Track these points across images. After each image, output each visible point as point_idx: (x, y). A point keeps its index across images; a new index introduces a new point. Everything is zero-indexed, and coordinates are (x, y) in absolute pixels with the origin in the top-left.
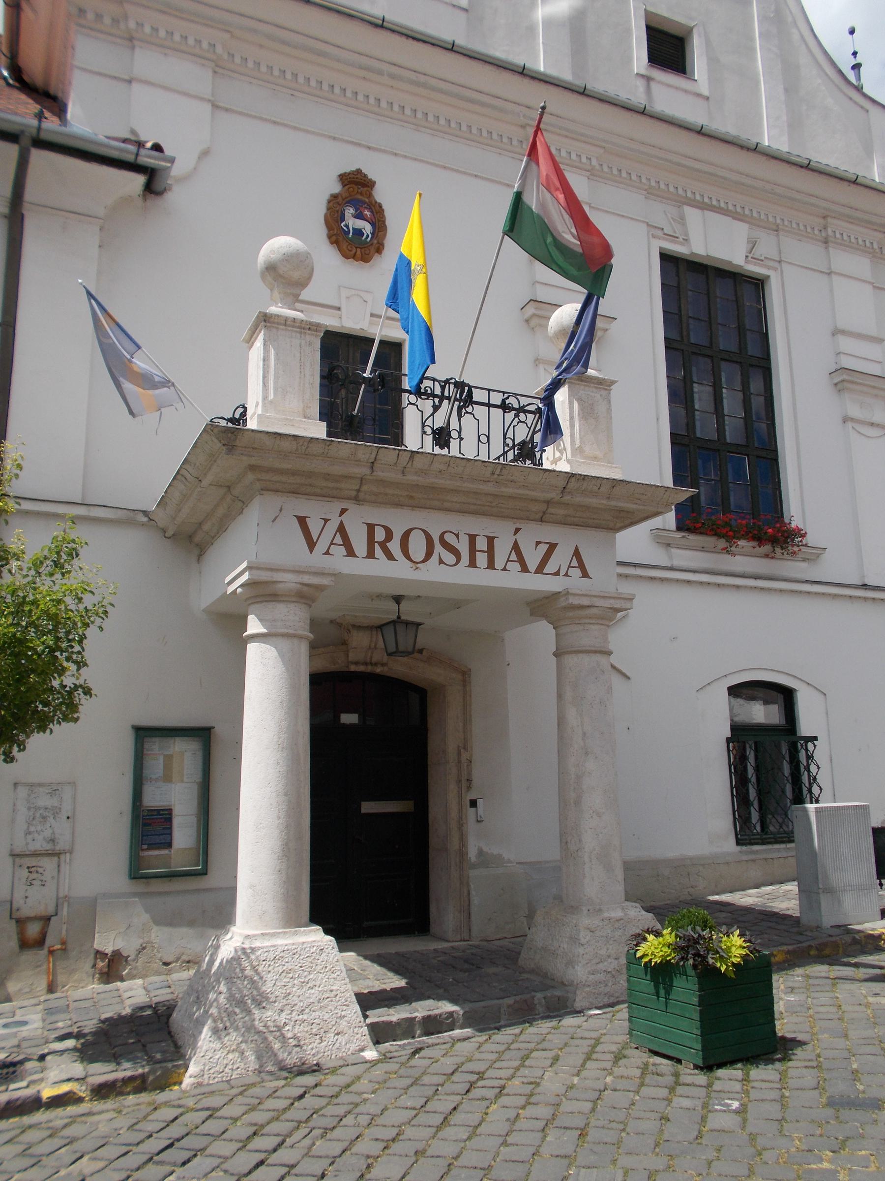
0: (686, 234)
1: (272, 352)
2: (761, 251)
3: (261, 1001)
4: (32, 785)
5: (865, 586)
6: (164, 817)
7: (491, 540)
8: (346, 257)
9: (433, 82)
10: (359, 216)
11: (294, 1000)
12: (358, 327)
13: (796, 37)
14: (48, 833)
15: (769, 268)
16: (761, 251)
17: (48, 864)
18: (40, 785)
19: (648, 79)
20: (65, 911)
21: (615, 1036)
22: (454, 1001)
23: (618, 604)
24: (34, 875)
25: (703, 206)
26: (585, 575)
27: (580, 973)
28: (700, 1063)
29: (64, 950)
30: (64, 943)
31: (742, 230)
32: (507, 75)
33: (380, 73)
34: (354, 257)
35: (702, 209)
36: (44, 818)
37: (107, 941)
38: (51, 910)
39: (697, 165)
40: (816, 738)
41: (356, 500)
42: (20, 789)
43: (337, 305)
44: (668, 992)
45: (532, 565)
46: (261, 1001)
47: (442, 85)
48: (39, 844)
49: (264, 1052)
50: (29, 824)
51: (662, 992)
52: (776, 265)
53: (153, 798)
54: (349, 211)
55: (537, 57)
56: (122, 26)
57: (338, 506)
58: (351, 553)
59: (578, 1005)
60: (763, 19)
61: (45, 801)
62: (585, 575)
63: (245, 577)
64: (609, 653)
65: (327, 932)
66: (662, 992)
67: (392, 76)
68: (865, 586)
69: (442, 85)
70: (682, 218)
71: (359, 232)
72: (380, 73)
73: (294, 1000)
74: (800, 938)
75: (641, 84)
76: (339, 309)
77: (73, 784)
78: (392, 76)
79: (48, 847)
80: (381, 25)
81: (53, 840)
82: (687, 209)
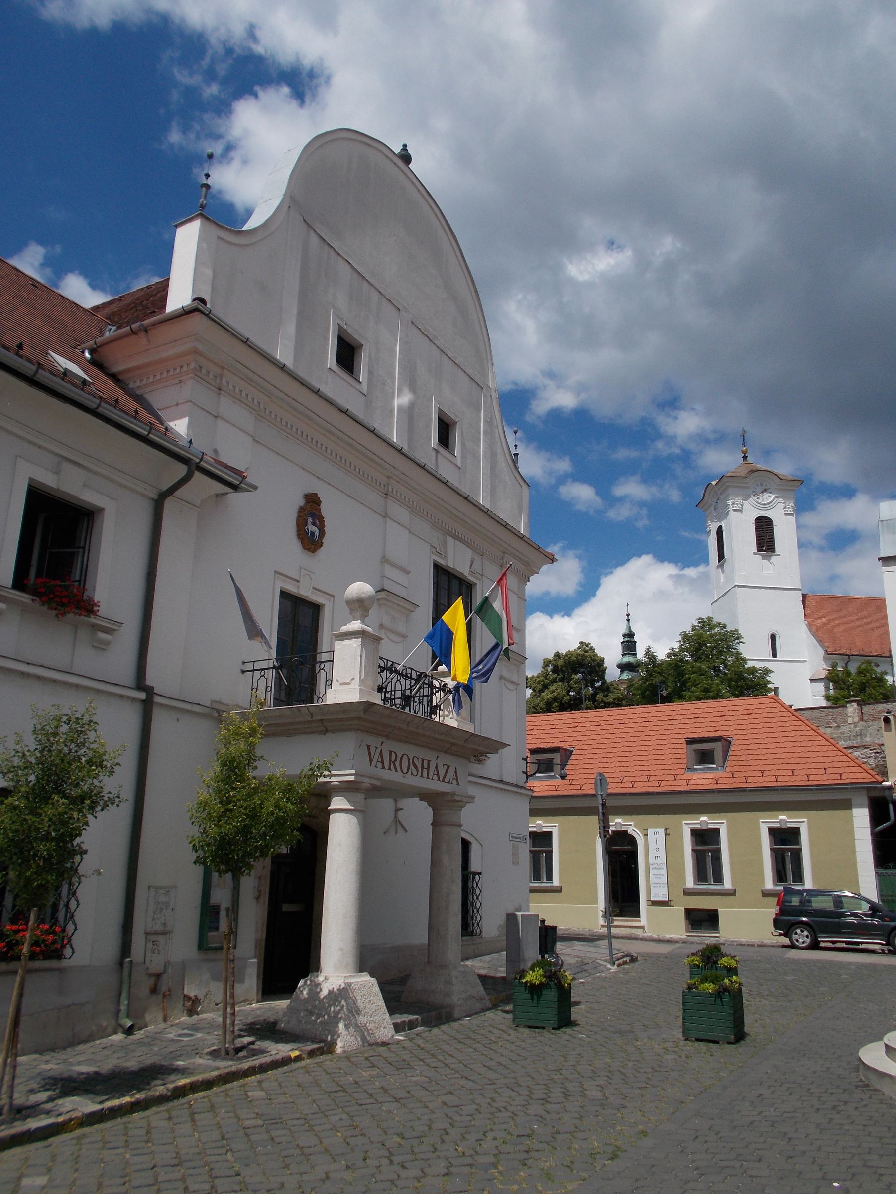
0: (446, 553)
1: (364, 652)
2: (477, 567)
3: (359, 1012)
4: (157, 888)
5: (501, 781)
6: (216, 910)
7: (429, 761)
8: (304, 548)
9: (377, 459)
10: (314, 524)
11: (368, 1010)
12: (305, 594)
13: (497, 435)
14: (162, 920)
15: (478, 578)
16: (477, 567)
17: (161, 939)
18: (161, 888)
19: (437, 451)
20: (170, 971)
21: (422, 1045)
22: (416, 1014)
23: (465, 800)
24: (155, 947)
25: (456, 537)
26: (458, 784)
27: (455, 999)
28: (556, 1026)
29: (170, 995)
30: (170, 990)
31: (469, 553)
32: (392, 449)
33: (334, 435)
34: (309, 550)
35: (455, 539)
36: (162, 909)
37: (191, 991)
38: (161, 970)
39: (458, 514)
40: (480, 873)
41: (388, 737)
42: (152, 889)
43: (297, 577)
44: (539, 997)
45: (441, 778)
46: (359, 1012)
47: (360, 447)
48: (158, 927)
49: (364, 1039)
50: (154, 913)
51: (535, 998)
52: (479, 576)
53: (214, 900)
54: (310, 520)
55: (392, 432)
56: (218, 381)
57: (381, 740)
58: (383, 767)
59: (456, 1015)
60: (485, 421)
61: (162, 899)
62: (458, 784)
63: (352, 778)
64: (461, 826)
65: (372, 976)
66: (535, 998)
67: (339, 438)
68: (501, 781)
69: (360, 447)
70: (445, 542)
71: (313, 534)
72: (334, 435)
73: (368, 1010)
74: (92, 1050)
75: (433, 453)
76: (298, 581)
77: (175, 887)
78: (339, 438)
79: (162, 928)
80: (346, 412)
81: (165, 925)
82: (448, 537)
